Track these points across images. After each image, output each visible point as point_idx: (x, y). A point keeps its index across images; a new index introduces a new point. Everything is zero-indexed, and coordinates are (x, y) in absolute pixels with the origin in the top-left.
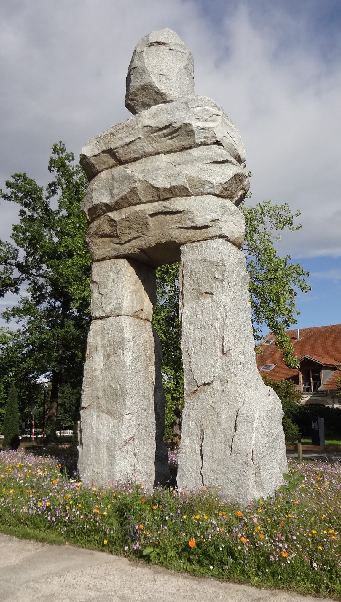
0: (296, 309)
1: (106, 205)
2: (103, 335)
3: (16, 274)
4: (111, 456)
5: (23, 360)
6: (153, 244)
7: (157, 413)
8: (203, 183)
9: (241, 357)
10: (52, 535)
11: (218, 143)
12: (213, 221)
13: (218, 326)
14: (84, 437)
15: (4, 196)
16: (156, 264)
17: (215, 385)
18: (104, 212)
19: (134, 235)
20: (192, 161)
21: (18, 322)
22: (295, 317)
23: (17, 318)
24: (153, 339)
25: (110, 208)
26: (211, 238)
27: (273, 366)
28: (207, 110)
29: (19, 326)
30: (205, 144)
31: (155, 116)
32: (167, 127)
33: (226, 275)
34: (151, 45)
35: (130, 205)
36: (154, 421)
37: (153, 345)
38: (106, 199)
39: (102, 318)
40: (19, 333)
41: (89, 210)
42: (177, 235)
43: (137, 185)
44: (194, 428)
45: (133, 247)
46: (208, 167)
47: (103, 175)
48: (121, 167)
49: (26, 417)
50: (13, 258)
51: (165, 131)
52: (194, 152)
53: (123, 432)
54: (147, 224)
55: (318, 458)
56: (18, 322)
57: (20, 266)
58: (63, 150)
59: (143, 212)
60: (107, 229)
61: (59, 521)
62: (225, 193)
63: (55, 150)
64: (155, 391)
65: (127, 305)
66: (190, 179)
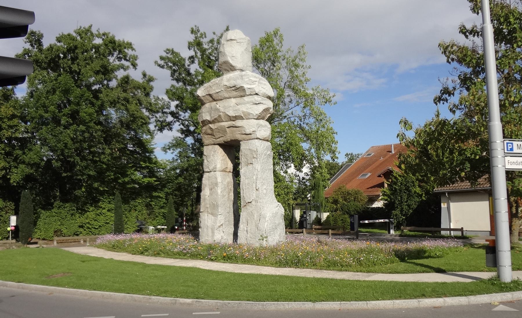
0: (338, 150)
1: (209, 121)
2: (209, 180)
3: (170, 118)
4: (213, 232)
5: (177, 178)
6: (229, 140)
7: (234, 214)
8: (249, 114)
9: (265, 191)
10: (185, 257)
11: (257, 94)
13: (255, 178)
14: (202, 225)
15: (159, 65)
16: (232, 149)
17: (253, 203)
18: (208, 124)
19: (221, 135)
20: (244, 104)
21: (172, 153)
22: (337, 155)
23: (172, 151)
24: (232, 181)
25: (210, 122)
26: (253, 139)
27: (369, 174)
29: (173, 156)
30: (251, 95)
31: (228, 80)
33: (258, 156)
34: (228, 41)
35: (219, 122)
36: (233, 217)
37: (232, 183)
38: (208, 118)
39: (208, 172)
40: (174, 160)
41: (202, 122)
42: (239, 137)
43: (221, 114)
44: (244, 221)
45: (221, 140)
47: (207, 105)
48: (215, 103)
49: (181, 215)
50: (168, 108)
51: (233, 88)
52: (246, 99)
53: (218, 222)
54: (226, 131)
55: (348, 238)
56: (172, 153)
57: (173, 114)
58: (198, 31)
59: (224, 126)
60: (209, 132)
61: (188, 253)
62: (259, 118)
63: (192, 32)
64: (233, 204)
65: (219, 166)
66: (243, 112)
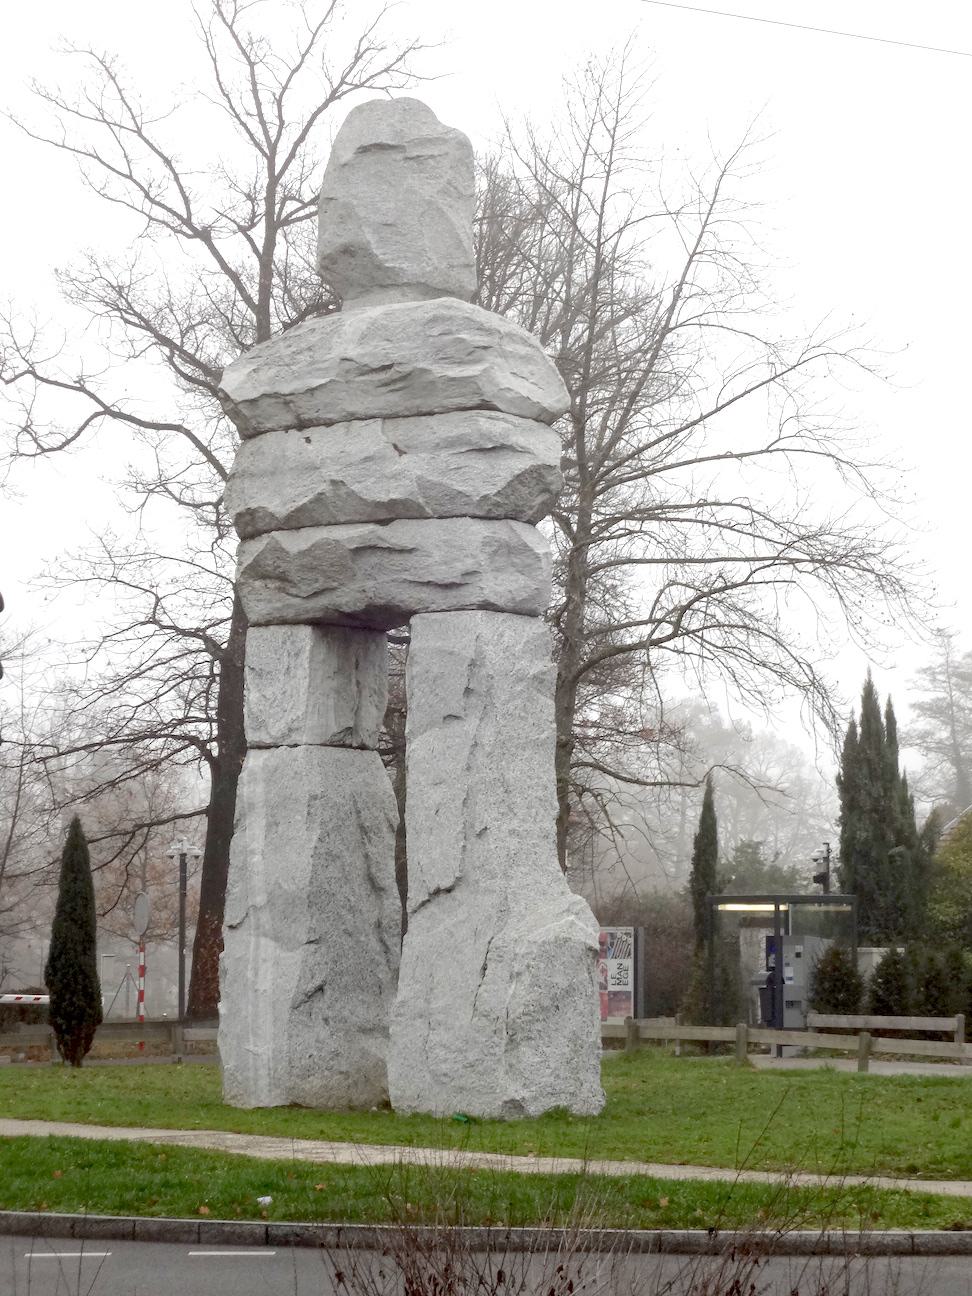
12: (467, 574)
28: (462, 341)
32: (384, 368)
42: (406, 597)
46: (462, 461)
